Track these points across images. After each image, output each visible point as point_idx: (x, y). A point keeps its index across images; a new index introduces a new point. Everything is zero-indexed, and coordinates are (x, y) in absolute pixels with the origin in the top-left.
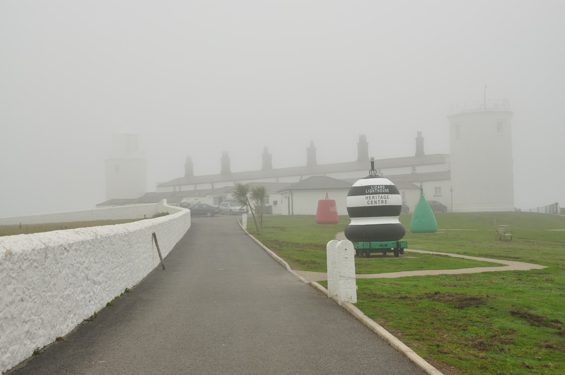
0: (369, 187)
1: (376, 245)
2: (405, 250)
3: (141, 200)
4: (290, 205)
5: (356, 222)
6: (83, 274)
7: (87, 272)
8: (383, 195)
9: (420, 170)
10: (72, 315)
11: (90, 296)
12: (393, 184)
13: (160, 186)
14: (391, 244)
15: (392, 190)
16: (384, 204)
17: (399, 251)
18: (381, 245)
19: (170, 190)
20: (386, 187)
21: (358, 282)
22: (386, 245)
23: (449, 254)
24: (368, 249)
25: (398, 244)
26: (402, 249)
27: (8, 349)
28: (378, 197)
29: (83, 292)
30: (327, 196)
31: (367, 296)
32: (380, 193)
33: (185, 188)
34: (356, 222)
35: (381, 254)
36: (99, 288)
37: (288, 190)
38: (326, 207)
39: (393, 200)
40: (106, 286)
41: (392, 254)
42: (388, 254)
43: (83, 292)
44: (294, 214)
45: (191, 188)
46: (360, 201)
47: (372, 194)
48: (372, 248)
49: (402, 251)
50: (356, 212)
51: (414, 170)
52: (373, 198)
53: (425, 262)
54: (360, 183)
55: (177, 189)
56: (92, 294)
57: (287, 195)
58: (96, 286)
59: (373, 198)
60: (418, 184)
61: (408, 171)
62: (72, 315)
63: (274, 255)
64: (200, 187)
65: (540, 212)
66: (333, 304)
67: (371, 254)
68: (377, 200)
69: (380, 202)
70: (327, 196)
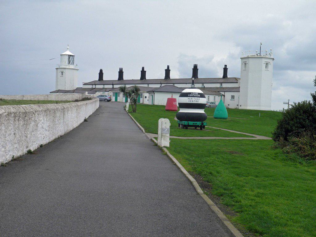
0: (190, 93)
1: (191, 123)
2: (205, 126)
3: (74, 91)
4: (153, 100)
5: (182, 111)
6: (41, 126)
7: (43, 125)
8: (197, 98)
9: (224, 85)
10: (35, 144)
11: (44, 136)
12: (202, 92)
13: (85, 84)
14: (199, 123)
15: (202, 96)
16: (197, 103)
17: (202, 127)
18: (194, 124)
19: (90, 87)
20: (199, 94)
21: (170, 139)
22: (196, 124)
23: (221, 129)
24: (187, 125)
25: (202, 124)
26: (204, 126)
27: (9, 153)
28: (194, 99)
29: (40, 134)
30: (172, 96)
31: (175, 147)
32: (195, 97)
33: (98, 86)
34: (182, 111)
35: (194, 128)
36: (48, 133)
37: (152, 91)
38: (171, 101)
39: (202, 101)
40: (51, 132)
41: (199, 128)
42: (197, 128)
43: (40, 134)
44: (220, 97)
45: (101, 86)
46: (185, 100)
47: (191, 97)
48: (189, 124)
49: (204, 127)
50: (183, 105)
51: (221, 85)
52: (192, 99)
53: (214, 133)
54: (186, 91)
55: (94, 87)
56: (45, 135)
57: (152, 94)
58: (47, 132)
59: (192, 99)
60: (223, 93)
61: (218, 85)
62: (35, 144)
63: (138, 124)
64: (106, 86)
65: (277, 111)
66: (160, 149)
67: (188, 128)
68: (194, 100)
69: (195, 101)
70: (172, 96)
